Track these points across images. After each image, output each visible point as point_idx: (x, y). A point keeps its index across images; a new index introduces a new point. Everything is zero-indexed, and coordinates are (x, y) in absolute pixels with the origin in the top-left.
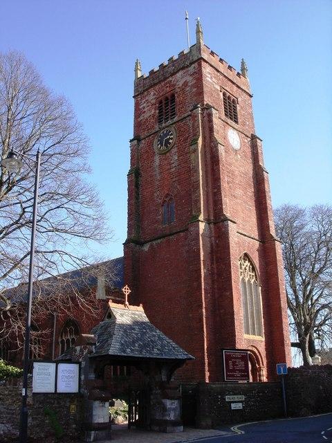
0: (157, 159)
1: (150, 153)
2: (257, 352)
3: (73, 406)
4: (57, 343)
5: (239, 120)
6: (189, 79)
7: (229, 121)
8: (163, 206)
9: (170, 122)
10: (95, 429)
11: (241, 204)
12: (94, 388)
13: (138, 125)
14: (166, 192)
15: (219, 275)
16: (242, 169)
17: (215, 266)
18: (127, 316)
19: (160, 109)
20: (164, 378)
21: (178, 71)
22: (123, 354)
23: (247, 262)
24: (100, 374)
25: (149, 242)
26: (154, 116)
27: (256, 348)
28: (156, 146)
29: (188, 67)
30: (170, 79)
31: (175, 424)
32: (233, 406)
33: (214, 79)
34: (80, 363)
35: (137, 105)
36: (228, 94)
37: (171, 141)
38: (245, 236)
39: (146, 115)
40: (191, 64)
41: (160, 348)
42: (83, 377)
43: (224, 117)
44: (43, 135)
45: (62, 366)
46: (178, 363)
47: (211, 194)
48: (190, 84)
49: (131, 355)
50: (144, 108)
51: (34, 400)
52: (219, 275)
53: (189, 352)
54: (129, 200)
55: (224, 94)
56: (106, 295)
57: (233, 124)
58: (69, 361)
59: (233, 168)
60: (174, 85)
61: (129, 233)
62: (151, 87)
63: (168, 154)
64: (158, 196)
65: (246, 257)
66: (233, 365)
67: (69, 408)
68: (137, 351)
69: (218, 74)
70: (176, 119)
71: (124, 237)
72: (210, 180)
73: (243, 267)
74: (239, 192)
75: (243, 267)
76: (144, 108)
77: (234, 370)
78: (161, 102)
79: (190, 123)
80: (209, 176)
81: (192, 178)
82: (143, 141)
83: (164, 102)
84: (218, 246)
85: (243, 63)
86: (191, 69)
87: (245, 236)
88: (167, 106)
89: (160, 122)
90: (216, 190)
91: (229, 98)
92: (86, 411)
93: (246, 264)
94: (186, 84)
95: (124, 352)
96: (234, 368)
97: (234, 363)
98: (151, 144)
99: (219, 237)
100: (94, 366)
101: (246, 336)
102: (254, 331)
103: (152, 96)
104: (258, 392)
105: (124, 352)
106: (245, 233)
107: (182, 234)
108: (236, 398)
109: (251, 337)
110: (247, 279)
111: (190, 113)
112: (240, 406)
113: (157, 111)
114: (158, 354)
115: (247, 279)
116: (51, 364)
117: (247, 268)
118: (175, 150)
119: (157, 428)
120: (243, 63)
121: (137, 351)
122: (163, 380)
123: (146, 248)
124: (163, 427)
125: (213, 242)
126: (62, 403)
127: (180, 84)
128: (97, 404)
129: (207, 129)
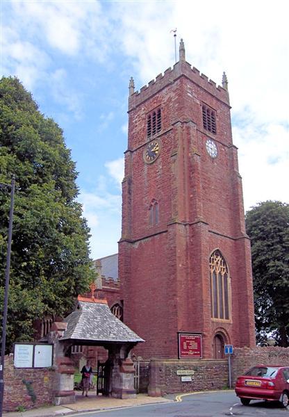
0: (146, 167)
1: (140, 163)
3: (46, 378)
5: (218, 131)
6: (173, 95)
7: (207, 133)
9: (157, 135)
10: (62, 396)
11: (215, 207)
12: (62, 364)
13: (131, 138)
14: (153, 197)
16: (218, 176)
17: (188, 262)
18: (92, 307)
20: (122, 356)
21: (163, 89)
22: (83, 338)
23: (219, 257)
24: (68, 354)
25: (138, 240)
26: (144, 129)
28: (145, 157)
29: (171, 84)
30: (157, 95)
31: (129, 392)
32: (183, 379)
33: (194, 94)
34: (52, 344)
35: (131, 119)
36: (207, 108)
37: (157, 152)
39: (138, 129)
40: (175, 81)
41: (115, 332)
42: (55, 356)
43: (202, 129)
44: (193, 103)
45: (38, 347)
46: (130, 346)
47: (187, 199)
48: (173, 100)
49: (90, 339)
50: (136, 122)
51: (14, 374)
53: (141, 337)
55: (203, 108)
57: (211, 135)
58: (46, 343)
59: (209, 175)
60: (160, 101)
61: (123, 233)
62: (142, 103)
63: (154, 164)
64: (147, 200)
65: (218, 253)
67: (42, 379)
68: (95, 335)
69: (199, 89)
70: (161, 133)
71: (119, 237)
72: (186, 186)
73: (215, 262)
74: (214, 196)
75: (215, 262)
76: (136, 122)
77: (188, 350)
79: (172, 135)
80: (186, 182)
81: (81, 217)
82: (135, 153)
83: (152, 117)
85: (225, 76)
86: (174, 86)
88: (155, 121)
90: (192, 196)
92: (55, 381)
93: (217, 259)
94: (170, 100)
95: (84, 336)
97: (188, 344)
98: (141, 155)
99: (193, 236)
100: (63, 348)
101: (214, 319)
103: (142, 112)
104: (207, 368)
105: (84, 336)
106: (218, 232)
107: (164, 234)
108: (186, 372)
109: (219, 320)
111: (172, 127)
112: (189, 379)
113: (147, 125)
114: (114, 338)
116: (29, 346)
117: (219, 262)
118: (160, 160)
119: (115, 395)
120: (225, 76)
121: (95, 335)
123: (136, 246)
124: (119, 394)
125: (188, 241)
126: (37, 376)
127: (165, 100)
128: (64, 376)
129: (186, 141)
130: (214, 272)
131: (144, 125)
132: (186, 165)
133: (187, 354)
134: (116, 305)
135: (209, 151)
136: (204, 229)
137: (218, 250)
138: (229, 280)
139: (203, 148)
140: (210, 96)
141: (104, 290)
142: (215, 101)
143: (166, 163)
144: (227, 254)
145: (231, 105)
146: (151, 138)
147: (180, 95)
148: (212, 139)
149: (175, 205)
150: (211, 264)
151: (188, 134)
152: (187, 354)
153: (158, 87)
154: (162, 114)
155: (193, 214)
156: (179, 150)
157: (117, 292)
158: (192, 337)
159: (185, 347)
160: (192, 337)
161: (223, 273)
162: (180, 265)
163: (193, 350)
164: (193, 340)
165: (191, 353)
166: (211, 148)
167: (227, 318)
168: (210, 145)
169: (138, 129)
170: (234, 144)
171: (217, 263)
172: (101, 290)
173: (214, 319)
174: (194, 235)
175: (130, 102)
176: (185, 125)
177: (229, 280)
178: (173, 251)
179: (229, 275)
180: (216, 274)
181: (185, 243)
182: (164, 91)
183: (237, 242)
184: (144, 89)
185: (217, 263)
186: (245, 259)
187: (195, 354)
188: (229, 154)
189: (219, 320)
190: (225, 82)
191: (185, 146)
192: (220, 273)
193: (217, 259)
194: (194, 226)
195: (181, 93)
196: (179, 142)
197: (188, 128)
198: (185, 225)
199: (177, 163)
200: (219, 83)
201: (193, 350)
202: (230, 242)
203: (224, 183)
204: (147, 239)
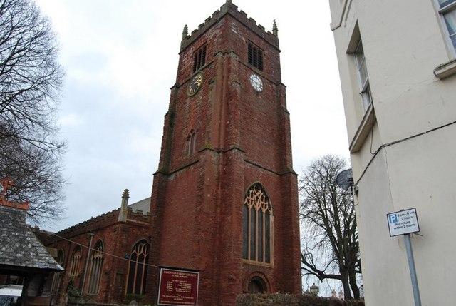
0: (188, 100)
2: (264, 279)
4: (90, 261)
7: (253, 68)
8: (188, 140)
11: (258, 139)
15: (224, 200)
17: (219, 192)
19: (195, 60)
27: (263, 274)
35: (181, 59)
38: (260, 167)
40: (221, 18)
43: (246, 62)
52: (224, 200)
54: (163, 137)
55: (250, 45)
56: (128, 217)
57: (257, 70)
65: (259, 187)
66: (174, 287)
71: (156, 168)
77: (174, 293)
78: (196, 55)
84: (225, 172)
85: (275, 25)
86: (220, 24)
87: (260, 167)
89: (194, 71)
90: (228, 122)
91: (254, 49)
93: (258, 193)
94: (215, 37)
96: (174, 290)
97: (175, 285)
101: (244, 260)
102: (255, 256)
103: (191, 52)
110: (257, 208)
115: (257, 208)
117: (260, 197)
120: (275, 25)
122: (29, 295)
127: (211, 37)
129: (225, 70)
130: (253, 208)
131: (191, 63)
132: (224, 93)
133: (172, 299)
134: (143, 241)
135: (254, 84)
136: (239, 158)
137: (258, 183)
138: (272, 218)
139: (247, 81)
140: (258, 37)
141: (128, 223)
142: (263, 42)
143: (206, 93)
144: (272, 191)
145: (280, 49)
146: (196, 72)
147: (223, 31)
148: (257, 74)
149: (209, 132)
150: (250, 198)
151: (229, 63)
152: (172, 299)
153: (205, 28)
154: (207, 51)
155: (227, 143)
156: (219, 77)
157: (146, 227)
158: (183, 275)
159: (170, 289)
160: (183, 275)
161: (264, 210)
162: (209, 195)
163: (183, 294)
164: (186, 279)
165: (179, 297)
166: (256, 82)
167: (268, 261)
168: (255, 79)
169: (185, 67)
170: (283, 82)
171: (257, 198)
172: (124, 223)
173: (250, 262)
174: (227, 162)
175: (182, 44)
176: (226, 55)
177: (272, 218)
178: (202, 179)
179: (271, 212)
180: (255, 211)
181: (216, 171)
182: (211, 30)
183: (283, 177)
184: (195, 32)
185: (257, 198)
186: (290, 196)
187: (185, 300)
188: (277, 91)
189: (257, 262)
190: (275, 29)
191: (225, 75)
192: (260, 209)
193: (258, 193)
194: (228, 152)
195: (226, 29)
196: (219, 71)
197: (229, 58)
198: (219, 152)
199: (214, 90)
200: (269, 28)
201: (183, 294)
202: (274, 178)
203: (270, 117)
204: (181, 171)
